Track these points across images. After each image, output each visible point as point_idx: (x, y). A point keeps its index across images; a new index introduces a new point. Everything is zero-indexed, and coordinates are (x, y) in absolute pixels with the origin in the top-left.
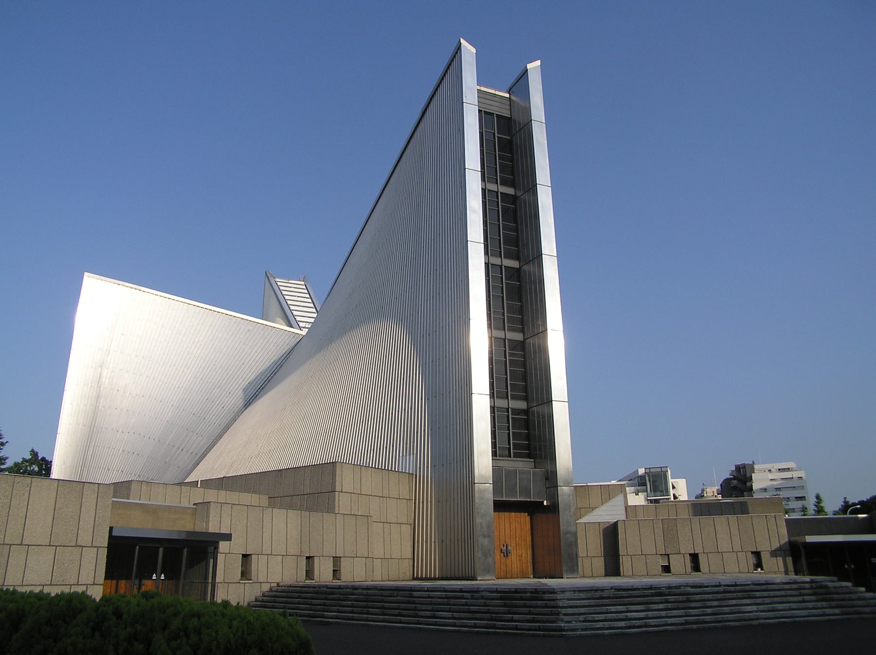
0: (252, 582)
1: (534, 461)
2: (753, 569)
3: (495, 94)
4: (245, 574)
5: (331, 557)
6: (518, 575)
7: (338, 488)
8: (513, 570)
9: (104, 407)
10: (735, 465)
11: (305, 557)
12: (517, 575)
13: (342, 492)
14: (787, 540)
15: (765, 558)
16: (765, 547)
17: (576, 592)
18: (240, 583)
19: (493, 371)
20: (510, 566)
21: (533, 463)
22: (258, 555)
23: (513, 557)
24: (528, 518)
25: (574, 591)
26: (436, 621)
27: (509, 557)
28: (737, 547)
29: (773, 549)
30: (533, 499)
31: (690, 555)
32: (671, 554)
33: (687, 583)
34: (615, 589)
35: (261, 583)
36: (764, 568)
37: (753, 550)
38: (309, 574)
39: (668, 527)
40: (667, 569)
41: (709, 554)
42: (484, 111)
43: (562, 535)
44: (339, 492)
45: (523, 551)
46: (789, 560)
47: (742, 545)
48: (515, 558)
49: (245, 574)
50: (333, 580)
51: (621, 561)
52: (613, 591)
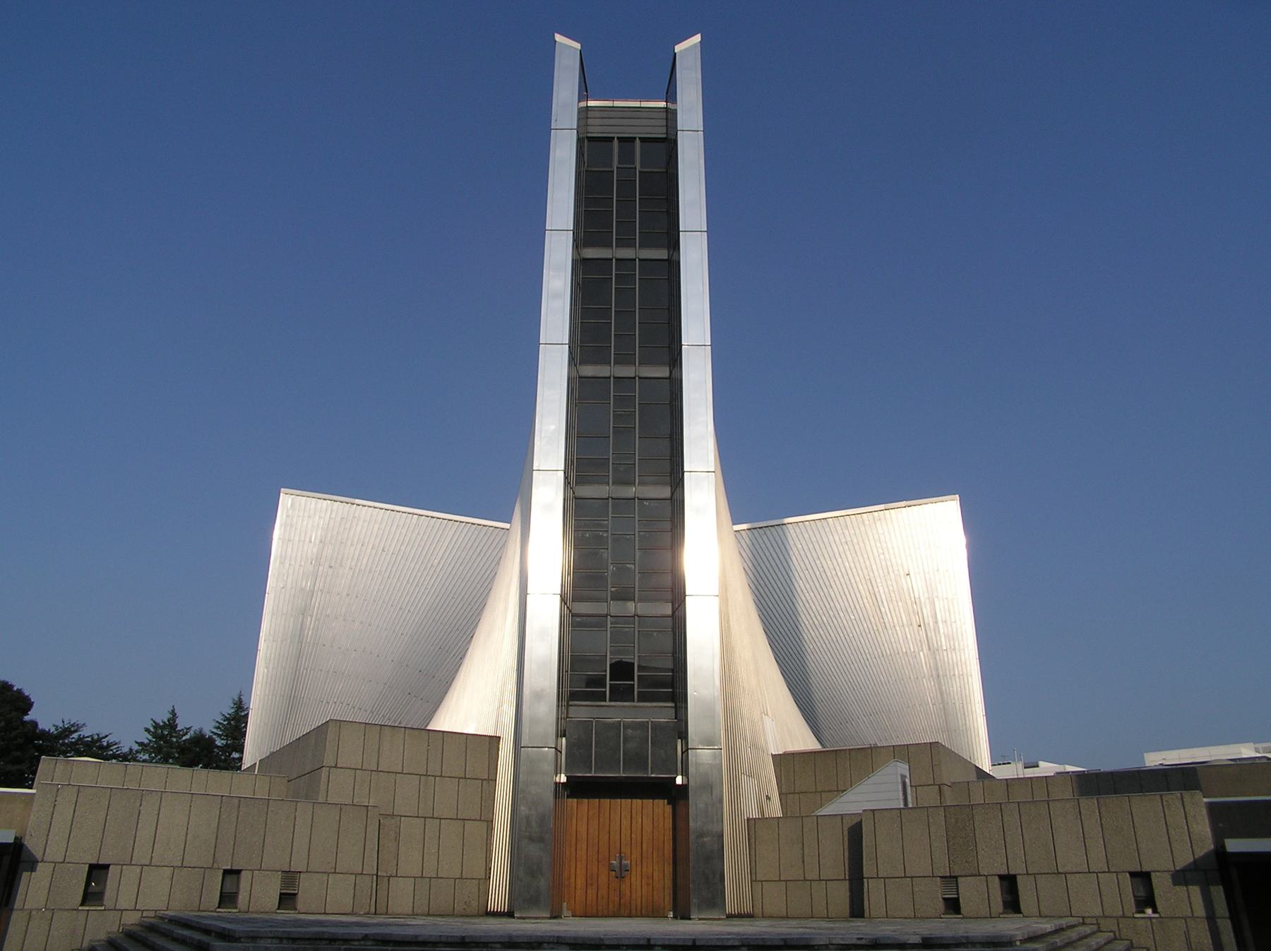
0: (103, 908)
1: (676, 704)
2: (1134, 911)
3: (613, 107)
4: (91, 896)
5: (278, 871)
6: (643, 912)
7: (329, 760)
8: (633, 902)
9: (335, 672)
11: (222, 871)
12: (641, 911)
13: (336, 767)
14: (1212, 847)
15: (1162, 885)
16: (1160, 863)
17: (285, 941)
20: (628, 893)
21: (674, 710)
22: (122, 865)
24: (669, 809)
25: (281, 939)
27: (627, 880)
28: (1098, 863)
29: (1178, 868)
30: (595, 773)
31: (1001, 877)
32: (962, 876)
34: (373, 940)
35: (122, 910)
36: (1160, 909)
37: (1133, 869)
38: (228, 898)
39: (957, 821)
40: (953, 906)
41: (1068, 876)
42: (618, 138)
43: (692, 837)
44: (331, 767)
46: (1218, 893)
47: (1109, 857)
48: (639, 882)
49: (91, 896)
50: (278, 909)
51: (865, 890)
52: (370, 943)
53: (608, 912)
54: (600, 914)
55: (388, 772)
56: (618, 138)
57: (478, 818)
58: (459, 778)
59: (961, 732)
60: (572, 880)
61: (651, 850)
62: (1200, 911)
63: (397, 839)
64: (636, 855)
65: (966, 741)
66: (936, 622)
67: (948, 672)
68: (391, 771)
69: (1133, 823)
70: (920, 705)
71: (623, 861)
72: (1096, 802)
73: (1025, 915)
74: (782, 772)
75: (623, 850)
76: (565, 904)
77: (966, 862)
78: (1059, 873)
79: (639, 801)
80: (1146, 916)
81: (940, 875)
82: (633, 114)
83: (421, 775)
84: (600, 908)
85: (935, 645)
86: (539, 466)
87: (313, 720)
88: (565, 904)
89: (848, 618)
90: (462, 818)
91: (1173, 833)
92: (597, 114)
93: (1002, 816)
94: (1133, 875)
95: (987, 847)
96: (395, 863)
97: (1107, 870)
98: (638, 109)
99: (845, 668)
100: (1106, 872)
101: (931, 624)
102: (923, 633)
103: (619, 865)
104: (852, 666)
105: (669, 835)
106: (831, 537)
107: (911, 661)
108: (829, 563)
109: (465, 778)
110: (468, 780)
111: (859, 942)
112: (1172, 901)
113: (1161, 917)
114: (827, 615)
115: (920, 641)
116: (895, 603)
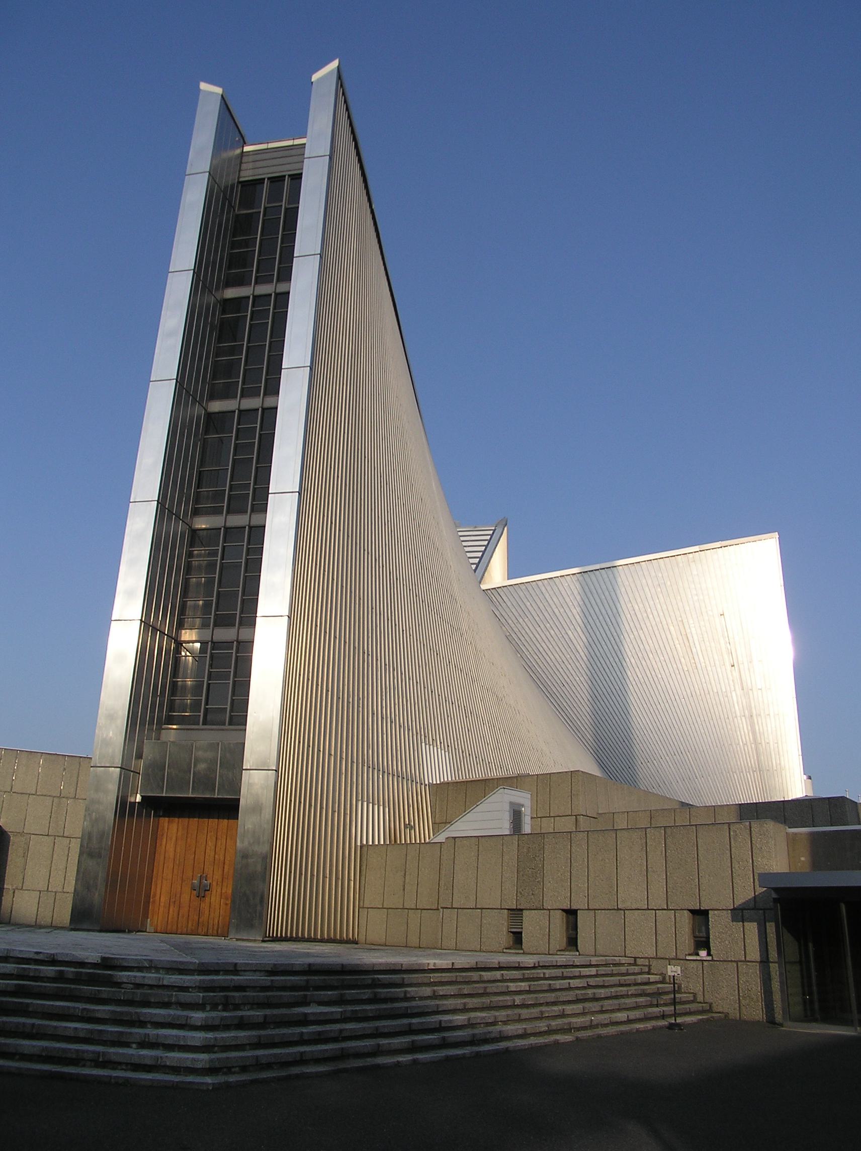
6: (219, 932)
8: (211, 922)
18: (503, 952)
20: (207, 912)
26: (76, 1029)
27: (207, 899)
28: (658, 901)
30: (166, 793)
33: (151, 961)
39: (528, 851)
40: (517, 938)
53: (187, 930)
54: (179, 931)
55: (22, 794)
56: (269, 179)
59: (775, 772)
62: (754, 954)
63: (25, 856)
64: (218, 876)
65: (780, 781)
67: (762, 712)
68: (24, 792)
69: (698, 855)
70: (744, 745)
72: (663, 832)
73: (581, 953)
74: (437, 801)
77: (533, 894)
78: (618, 909)
80: (698, 958)
81: (507, 908)
82: (287, 153)
83: (54, 797)
84: (179, 926)
86: (135, 498)
87: (725, 791)
89: (657, 659)
91: (737, 867)
92: (251, 158)
93: (571, 846)
94: (693, 912)
95: (553, 878)
96: (21, 877)
97: (666, 908)
98: (292, 147)
99: (651, 708)
100: (665, 909)
102: (736, 674)
104: (659, 706)
106: (644, 581)
107: (722, 700)
108: (641, 606)
111: (37, 957)
112: (727, 942)
113: (712, 960)
114: (636, 657)
115: (733, 681)
116: (708, 644)
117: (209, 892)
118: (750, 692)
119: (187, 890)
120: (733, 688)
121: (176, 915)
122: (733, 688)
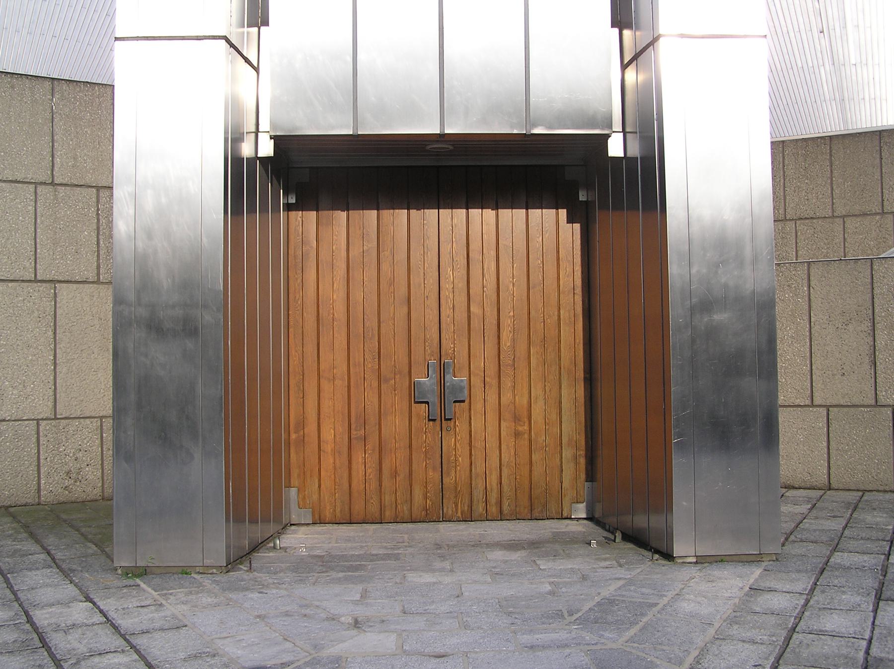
6: (506, 507)
10: (567, 223)
12: (500, 503)
19: (244, 13)
20: (463, 461)
23: (477, 424)
24: (571, 233)
27: (461, 426)
43: (676, 312)
45: (537, 391)
48: (492, 427)
57: (92, 276)
58: (36, 184)
60: (311, 428)
61: (522, 347)
66: (845, 27)
71: (448, 377)
75: (447, 345)
76: (293, 491)
79: (489, 214)
84: (388, 499)
85: (841, 57)
88: (293, 491)
90: (48, 277)
101: (838, 30)
102: (825, 42)
103: (436, 388)
105: (573, 302)
109: (52, 184)
110: (61, 189)
117: (465, 405)
118: (842, 68)
119: (397, 402)
120: (821, 63)
121: (372, 472)
122: (821, 63)
